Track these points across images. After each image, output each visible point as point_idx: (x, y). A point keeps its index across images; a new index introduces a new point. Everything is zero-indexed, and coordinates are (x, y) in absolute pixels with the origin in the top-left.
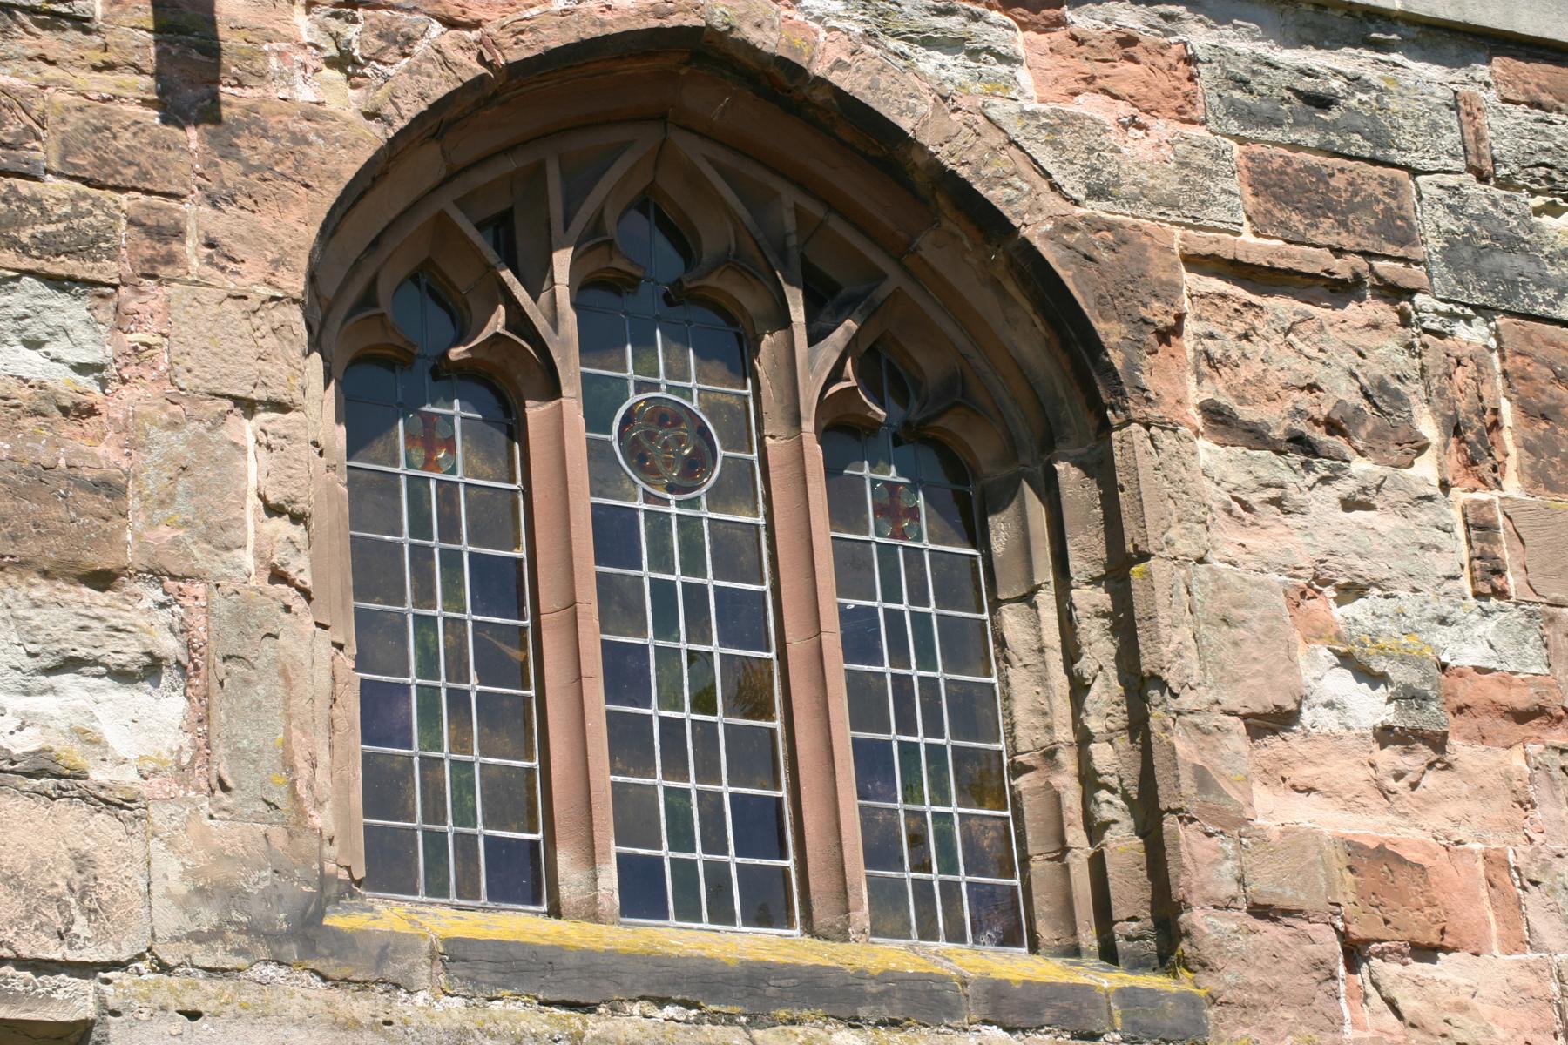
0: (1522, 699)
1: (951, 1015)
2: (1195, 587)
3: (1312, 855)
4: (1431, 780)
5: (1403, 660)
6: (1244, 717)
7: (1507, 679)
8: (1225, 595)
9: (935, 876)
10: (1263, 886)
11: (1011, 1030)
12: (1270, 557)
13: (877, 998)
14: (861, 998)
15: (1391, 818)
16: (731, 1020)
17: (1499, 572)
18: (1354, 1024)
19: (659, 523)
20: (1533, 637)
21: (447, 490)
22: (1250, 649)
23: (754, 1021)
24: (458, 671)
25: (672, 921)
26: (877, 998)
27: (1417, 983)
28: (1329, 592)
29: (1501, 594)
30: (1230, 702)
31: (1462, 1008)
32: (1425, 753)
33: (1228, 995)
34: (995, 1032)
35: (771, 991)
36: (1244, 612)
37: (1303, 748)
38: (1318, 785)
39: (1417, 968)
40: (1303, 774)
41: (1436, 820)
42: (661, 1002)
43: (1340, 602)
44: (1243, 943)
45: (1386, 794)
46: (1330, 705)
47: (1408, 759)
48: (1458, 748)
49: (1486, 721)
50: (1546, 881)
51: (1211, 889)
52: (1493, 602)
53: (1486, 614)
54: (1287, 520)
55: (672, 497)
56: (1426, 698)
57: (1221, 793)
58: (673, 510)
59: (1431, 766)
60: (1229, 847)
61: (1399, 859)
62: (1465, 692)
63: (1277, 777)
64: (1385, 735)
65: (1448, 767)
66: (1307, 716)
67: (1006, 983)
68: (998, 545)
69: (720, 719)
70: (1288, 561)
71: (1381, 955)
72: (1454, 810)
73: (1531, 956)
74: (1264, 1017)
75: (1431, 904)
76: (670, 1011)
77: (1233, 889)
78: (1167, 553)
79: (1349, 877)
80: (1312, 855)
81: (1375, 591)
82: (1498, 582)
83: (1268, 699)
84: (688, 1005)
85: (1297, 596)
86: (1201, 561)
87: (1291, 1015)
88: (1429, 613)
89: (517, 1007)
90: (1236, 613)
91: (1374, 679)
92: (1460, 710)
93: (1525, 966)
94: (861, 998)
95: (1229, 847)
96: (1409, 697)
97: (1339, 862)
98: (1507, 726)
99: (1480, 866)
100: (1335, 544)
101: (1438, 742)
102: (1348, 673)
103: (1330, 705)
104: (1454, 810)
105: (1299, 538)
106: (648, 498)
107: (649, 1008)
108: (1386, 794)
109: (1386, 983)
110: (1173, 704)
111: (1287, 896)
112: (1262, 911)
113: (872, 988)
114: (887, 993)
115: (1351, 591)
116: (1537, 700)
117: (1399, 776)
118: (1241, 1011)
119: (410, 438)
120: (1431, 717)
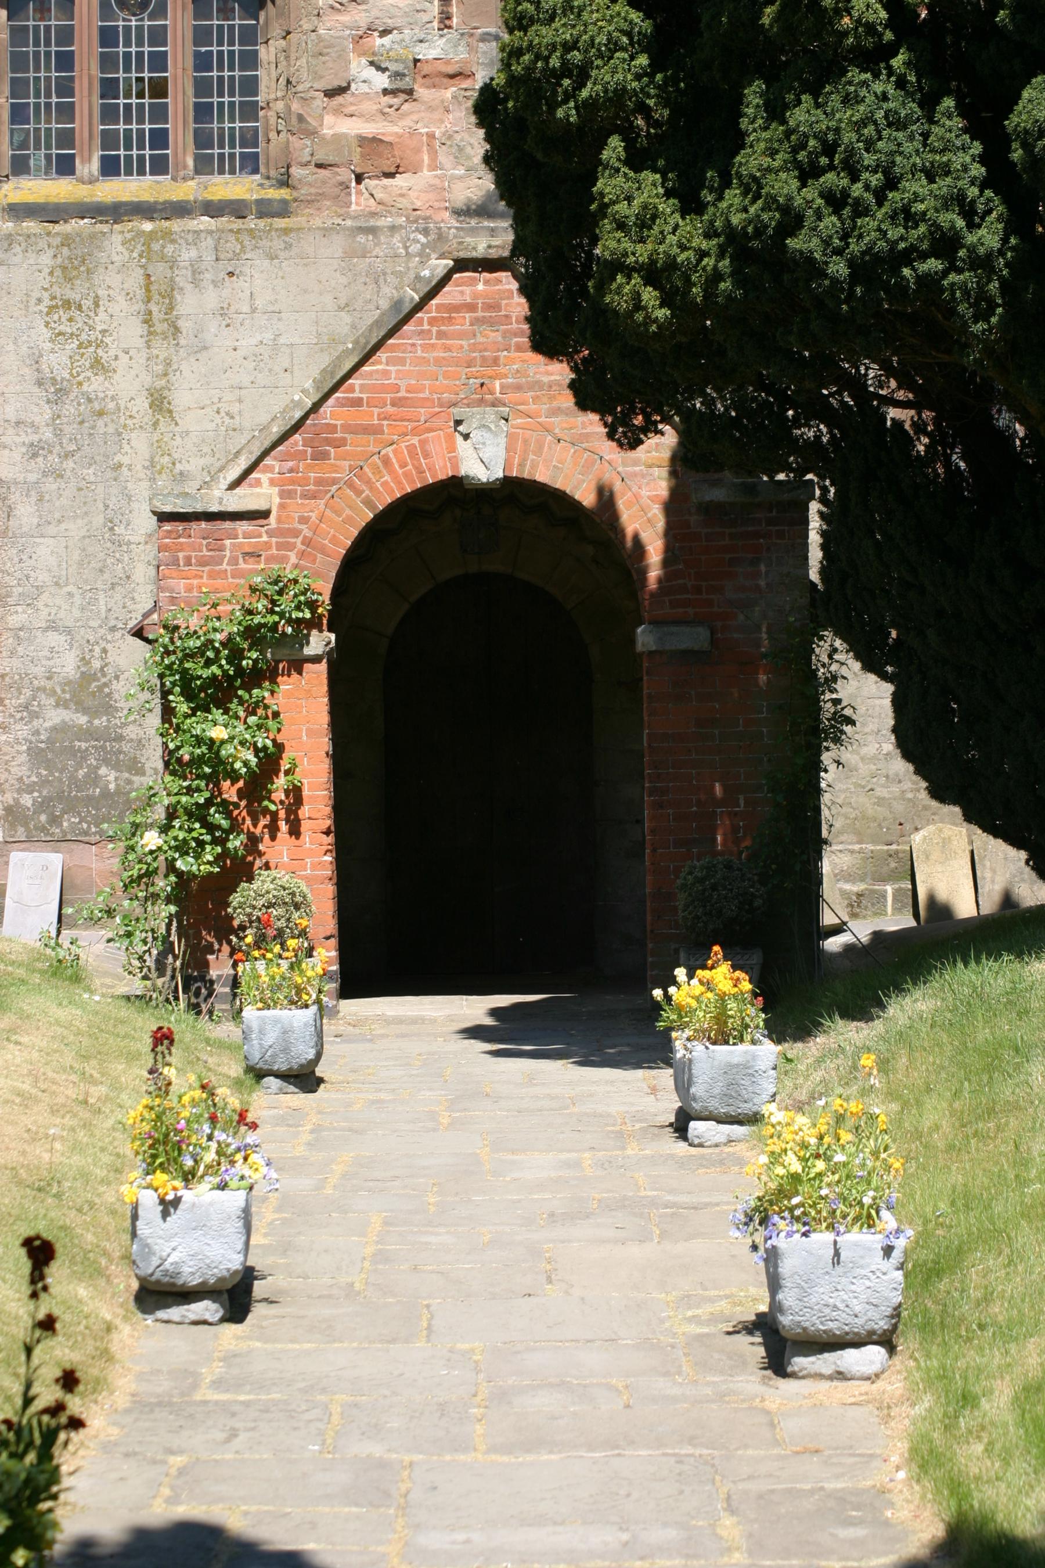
0: (451, 70)
1: (189, 214)
2: (309, 42)
3: (343, 142)
4: (406, 107)
5: (396, 61)
6: (324, 91)
7: (448, 62)
8: (322, 44)
9: (227, 150)
10: (320, 157)
11: (212, 217)
12: (348, 24)
13: (161, 210)
14: (155, 211)
15: (385, 123)
16: (107, 222)
17: (449, 18)
18: (357, 204)
19: (127, 29)
20: (463, 43)
21: (48, 28)
22: (330, 65)
23: (115, 222)
24: (48, 95)
25: (123, 177)
26: (161, 210)
27: (385, 187)
28: (376, 34)
29: (450, 27)
30: (316, 86)
31: (402, 195)
32: (403, 97)
33: (302, 198)
34: (206, 218)
35: (122, 211)
36: (328, 50)
37: (351, 99)
38: (356, 113)
39: (386, 181)
40: (351, 109)
41: (407, 122)
42: (83, 218)
43: (381, 36)
44: (310, 179)
45: (384, 114)
46: (365, 81)
47: (395, 100)
48: (421, 91)
49: (437, 80)
50: (448, 143)
51: (300, 159)
52: (446, 31)
53: (442, 36)
54: (360, 7)
55: (133, 18)
56: (404, 75)
57: (308, 123)
58: (134, 23)
59: (406, 101)
60: (309, 143)
61: (381, 141)
62: (426, 69)
63: (338, 111)
64: (386, 92)
65: (415, 100)
66: (353, 86)
67: (212, 201)
68: (262, 20)
69: (236, 48)
70: (356, 25)
71: (369, 178)
72: (415, 117)
73: (439, 172)
74: (317, 205)
75: (394, 156)
76: (86, 220)
77: (309, 158)
78: (299, 30)
79: (359, 149)
80: (343, 142)
81: (395, 32)
82: (447, 22)
83: (336, 83)
84: (93, 218)
85: (357, 39)
86: (313, 31)
87: (328, 203)
88: (415, 38)
89: (32, 224)
90: (325, 51)
91: (384, 70)
92: (424, 77)
93: (436, 176)
94: (155, 211)
95: (309, 143)
96: (398, 75)
97: (354, 143)
98: (446, 80)
99: (425, 138)
100: (379, 14)
101: (410, 92)
102: (373, 68)
103: (365, 81)
104: (415, 117)
105: (363, 14)
106: (124, 20)
107: (78, 220)
108: (384, 114)
109: (370, 188)
110: (294, 90)
111: (331, 159)
112: (319, 166)
113: (160, 207)
114: (165, 208)
115: (385, 33)
116: (459, 69)
117: (391, 107)
118: (125, 269)
119: (34, 10)
120: (405, 83)
